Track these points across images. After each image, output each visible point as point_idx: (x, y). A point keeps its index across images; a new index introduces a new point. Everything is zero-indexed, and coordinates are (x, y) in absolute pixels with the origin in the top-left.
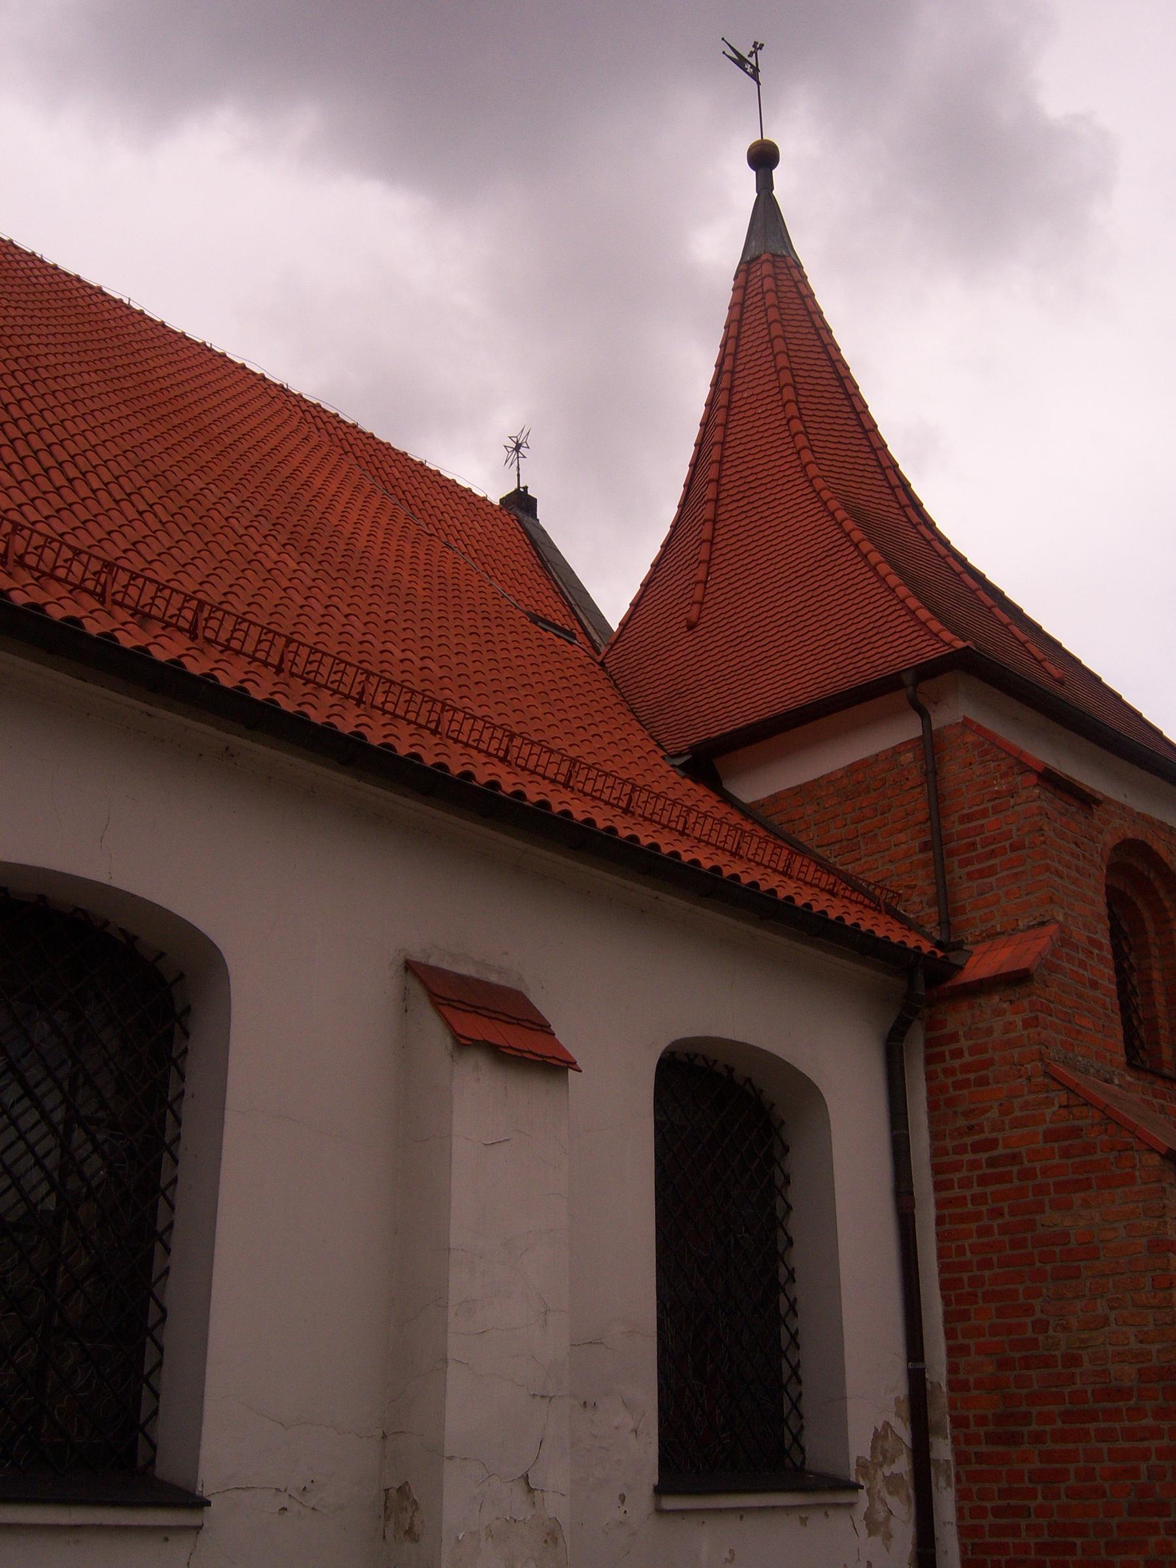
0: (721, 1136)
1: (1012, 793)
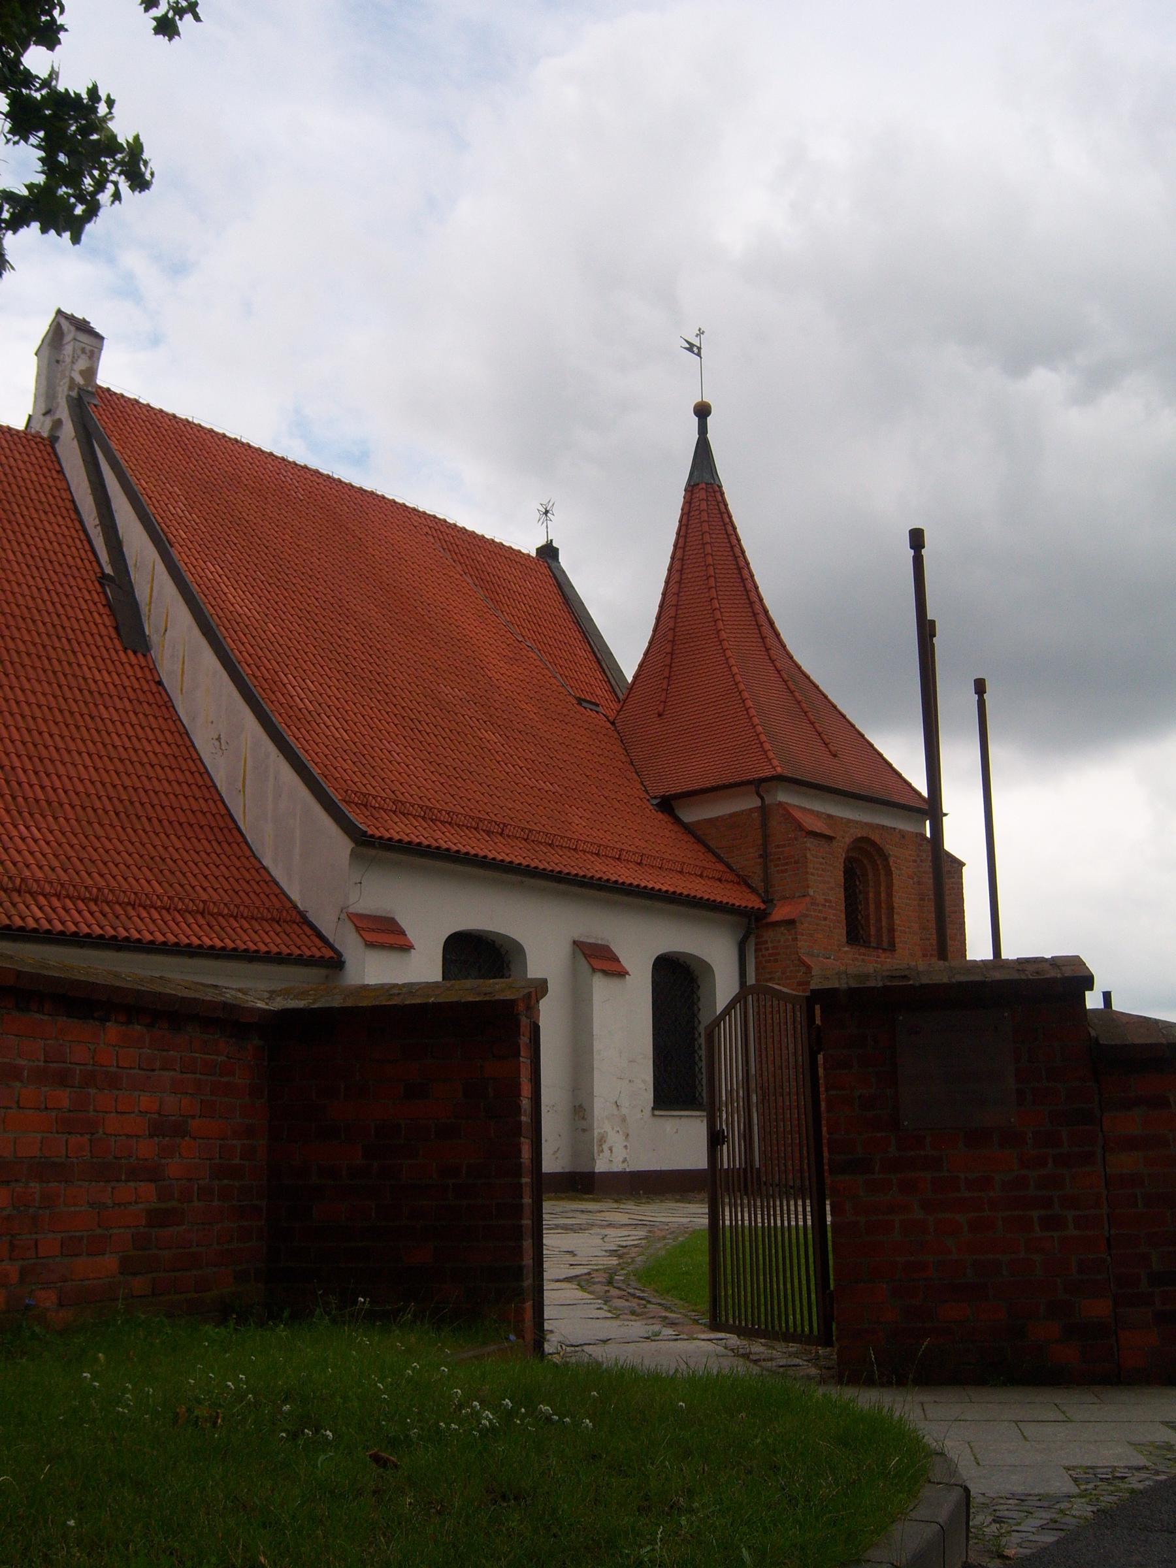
0: (676, 980)
1: (796, 839)
